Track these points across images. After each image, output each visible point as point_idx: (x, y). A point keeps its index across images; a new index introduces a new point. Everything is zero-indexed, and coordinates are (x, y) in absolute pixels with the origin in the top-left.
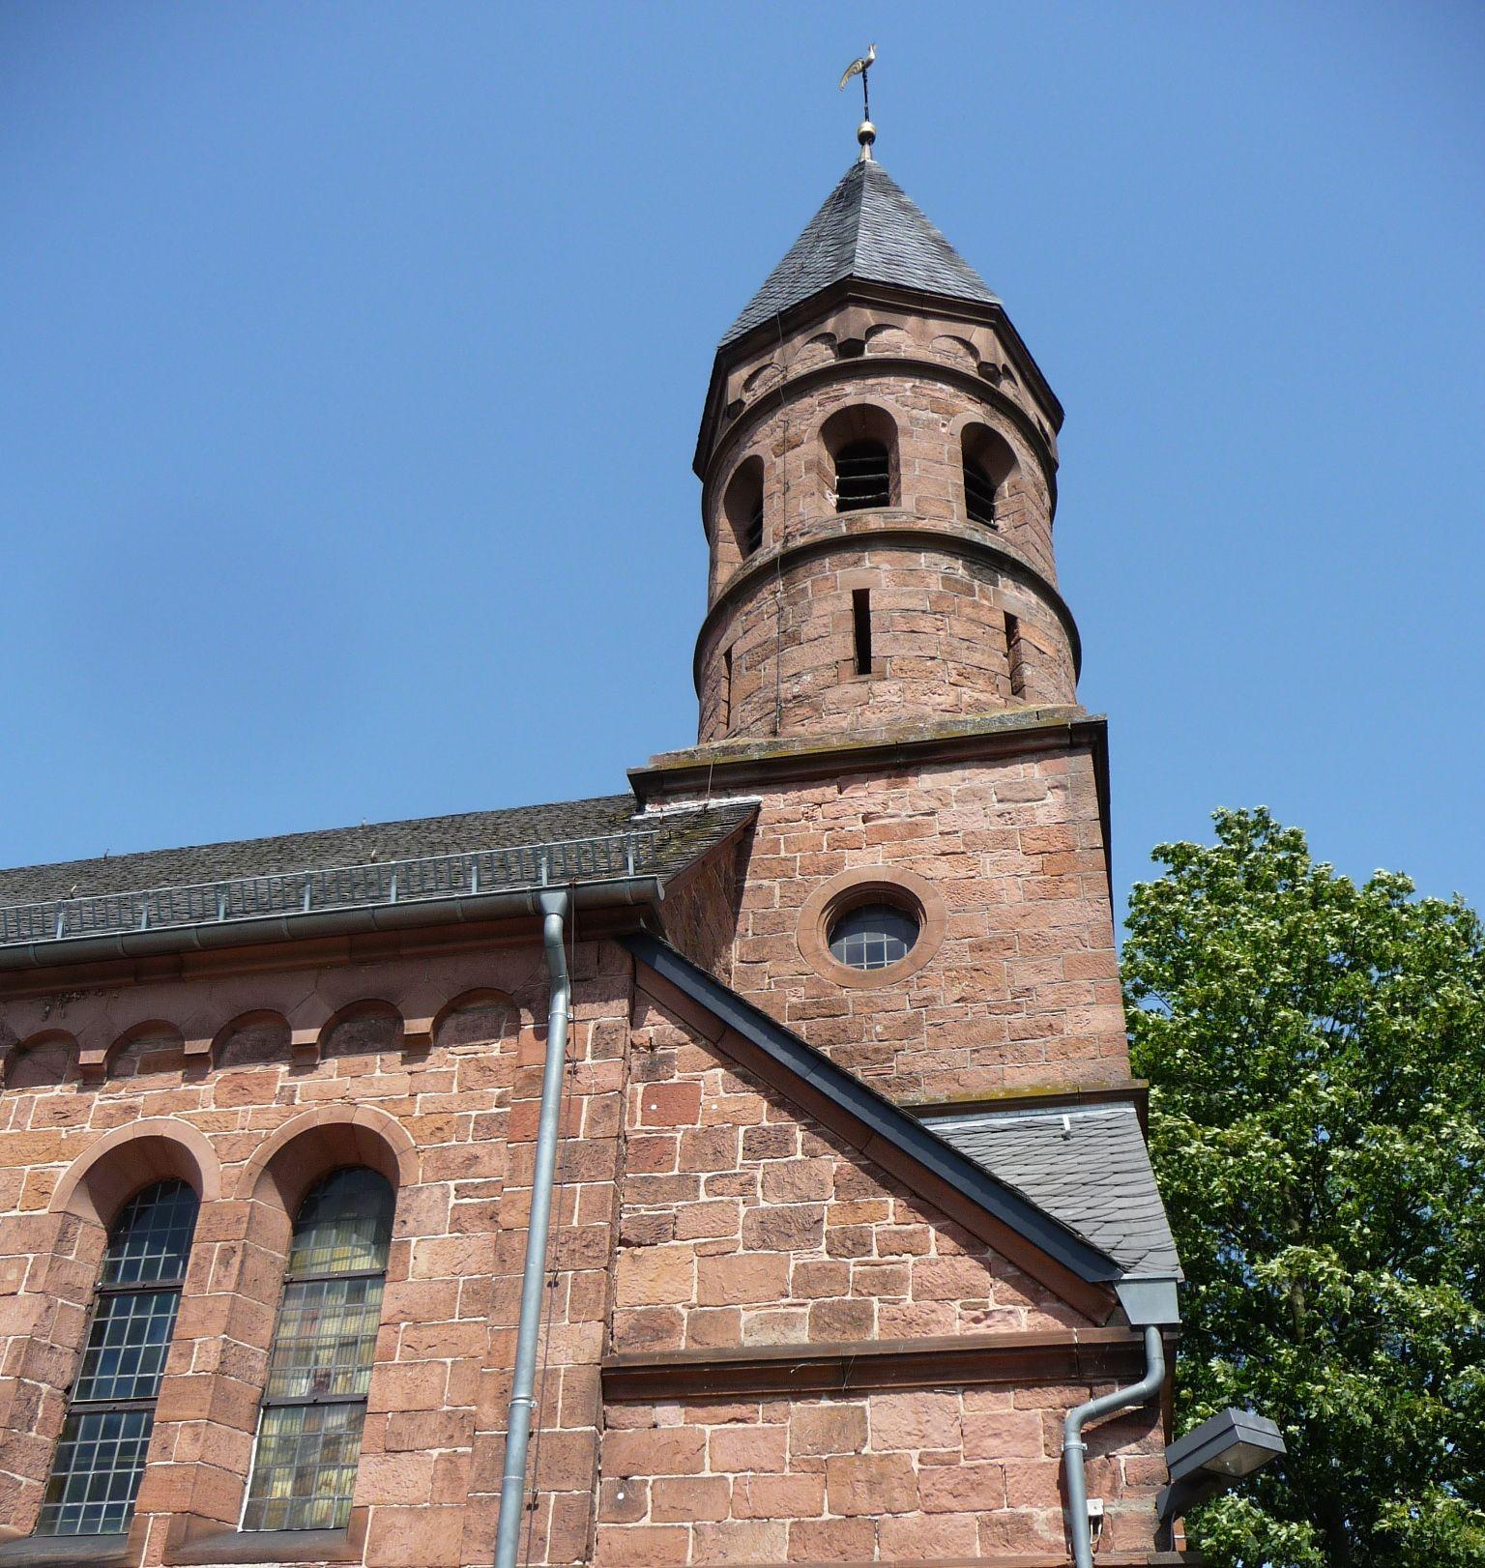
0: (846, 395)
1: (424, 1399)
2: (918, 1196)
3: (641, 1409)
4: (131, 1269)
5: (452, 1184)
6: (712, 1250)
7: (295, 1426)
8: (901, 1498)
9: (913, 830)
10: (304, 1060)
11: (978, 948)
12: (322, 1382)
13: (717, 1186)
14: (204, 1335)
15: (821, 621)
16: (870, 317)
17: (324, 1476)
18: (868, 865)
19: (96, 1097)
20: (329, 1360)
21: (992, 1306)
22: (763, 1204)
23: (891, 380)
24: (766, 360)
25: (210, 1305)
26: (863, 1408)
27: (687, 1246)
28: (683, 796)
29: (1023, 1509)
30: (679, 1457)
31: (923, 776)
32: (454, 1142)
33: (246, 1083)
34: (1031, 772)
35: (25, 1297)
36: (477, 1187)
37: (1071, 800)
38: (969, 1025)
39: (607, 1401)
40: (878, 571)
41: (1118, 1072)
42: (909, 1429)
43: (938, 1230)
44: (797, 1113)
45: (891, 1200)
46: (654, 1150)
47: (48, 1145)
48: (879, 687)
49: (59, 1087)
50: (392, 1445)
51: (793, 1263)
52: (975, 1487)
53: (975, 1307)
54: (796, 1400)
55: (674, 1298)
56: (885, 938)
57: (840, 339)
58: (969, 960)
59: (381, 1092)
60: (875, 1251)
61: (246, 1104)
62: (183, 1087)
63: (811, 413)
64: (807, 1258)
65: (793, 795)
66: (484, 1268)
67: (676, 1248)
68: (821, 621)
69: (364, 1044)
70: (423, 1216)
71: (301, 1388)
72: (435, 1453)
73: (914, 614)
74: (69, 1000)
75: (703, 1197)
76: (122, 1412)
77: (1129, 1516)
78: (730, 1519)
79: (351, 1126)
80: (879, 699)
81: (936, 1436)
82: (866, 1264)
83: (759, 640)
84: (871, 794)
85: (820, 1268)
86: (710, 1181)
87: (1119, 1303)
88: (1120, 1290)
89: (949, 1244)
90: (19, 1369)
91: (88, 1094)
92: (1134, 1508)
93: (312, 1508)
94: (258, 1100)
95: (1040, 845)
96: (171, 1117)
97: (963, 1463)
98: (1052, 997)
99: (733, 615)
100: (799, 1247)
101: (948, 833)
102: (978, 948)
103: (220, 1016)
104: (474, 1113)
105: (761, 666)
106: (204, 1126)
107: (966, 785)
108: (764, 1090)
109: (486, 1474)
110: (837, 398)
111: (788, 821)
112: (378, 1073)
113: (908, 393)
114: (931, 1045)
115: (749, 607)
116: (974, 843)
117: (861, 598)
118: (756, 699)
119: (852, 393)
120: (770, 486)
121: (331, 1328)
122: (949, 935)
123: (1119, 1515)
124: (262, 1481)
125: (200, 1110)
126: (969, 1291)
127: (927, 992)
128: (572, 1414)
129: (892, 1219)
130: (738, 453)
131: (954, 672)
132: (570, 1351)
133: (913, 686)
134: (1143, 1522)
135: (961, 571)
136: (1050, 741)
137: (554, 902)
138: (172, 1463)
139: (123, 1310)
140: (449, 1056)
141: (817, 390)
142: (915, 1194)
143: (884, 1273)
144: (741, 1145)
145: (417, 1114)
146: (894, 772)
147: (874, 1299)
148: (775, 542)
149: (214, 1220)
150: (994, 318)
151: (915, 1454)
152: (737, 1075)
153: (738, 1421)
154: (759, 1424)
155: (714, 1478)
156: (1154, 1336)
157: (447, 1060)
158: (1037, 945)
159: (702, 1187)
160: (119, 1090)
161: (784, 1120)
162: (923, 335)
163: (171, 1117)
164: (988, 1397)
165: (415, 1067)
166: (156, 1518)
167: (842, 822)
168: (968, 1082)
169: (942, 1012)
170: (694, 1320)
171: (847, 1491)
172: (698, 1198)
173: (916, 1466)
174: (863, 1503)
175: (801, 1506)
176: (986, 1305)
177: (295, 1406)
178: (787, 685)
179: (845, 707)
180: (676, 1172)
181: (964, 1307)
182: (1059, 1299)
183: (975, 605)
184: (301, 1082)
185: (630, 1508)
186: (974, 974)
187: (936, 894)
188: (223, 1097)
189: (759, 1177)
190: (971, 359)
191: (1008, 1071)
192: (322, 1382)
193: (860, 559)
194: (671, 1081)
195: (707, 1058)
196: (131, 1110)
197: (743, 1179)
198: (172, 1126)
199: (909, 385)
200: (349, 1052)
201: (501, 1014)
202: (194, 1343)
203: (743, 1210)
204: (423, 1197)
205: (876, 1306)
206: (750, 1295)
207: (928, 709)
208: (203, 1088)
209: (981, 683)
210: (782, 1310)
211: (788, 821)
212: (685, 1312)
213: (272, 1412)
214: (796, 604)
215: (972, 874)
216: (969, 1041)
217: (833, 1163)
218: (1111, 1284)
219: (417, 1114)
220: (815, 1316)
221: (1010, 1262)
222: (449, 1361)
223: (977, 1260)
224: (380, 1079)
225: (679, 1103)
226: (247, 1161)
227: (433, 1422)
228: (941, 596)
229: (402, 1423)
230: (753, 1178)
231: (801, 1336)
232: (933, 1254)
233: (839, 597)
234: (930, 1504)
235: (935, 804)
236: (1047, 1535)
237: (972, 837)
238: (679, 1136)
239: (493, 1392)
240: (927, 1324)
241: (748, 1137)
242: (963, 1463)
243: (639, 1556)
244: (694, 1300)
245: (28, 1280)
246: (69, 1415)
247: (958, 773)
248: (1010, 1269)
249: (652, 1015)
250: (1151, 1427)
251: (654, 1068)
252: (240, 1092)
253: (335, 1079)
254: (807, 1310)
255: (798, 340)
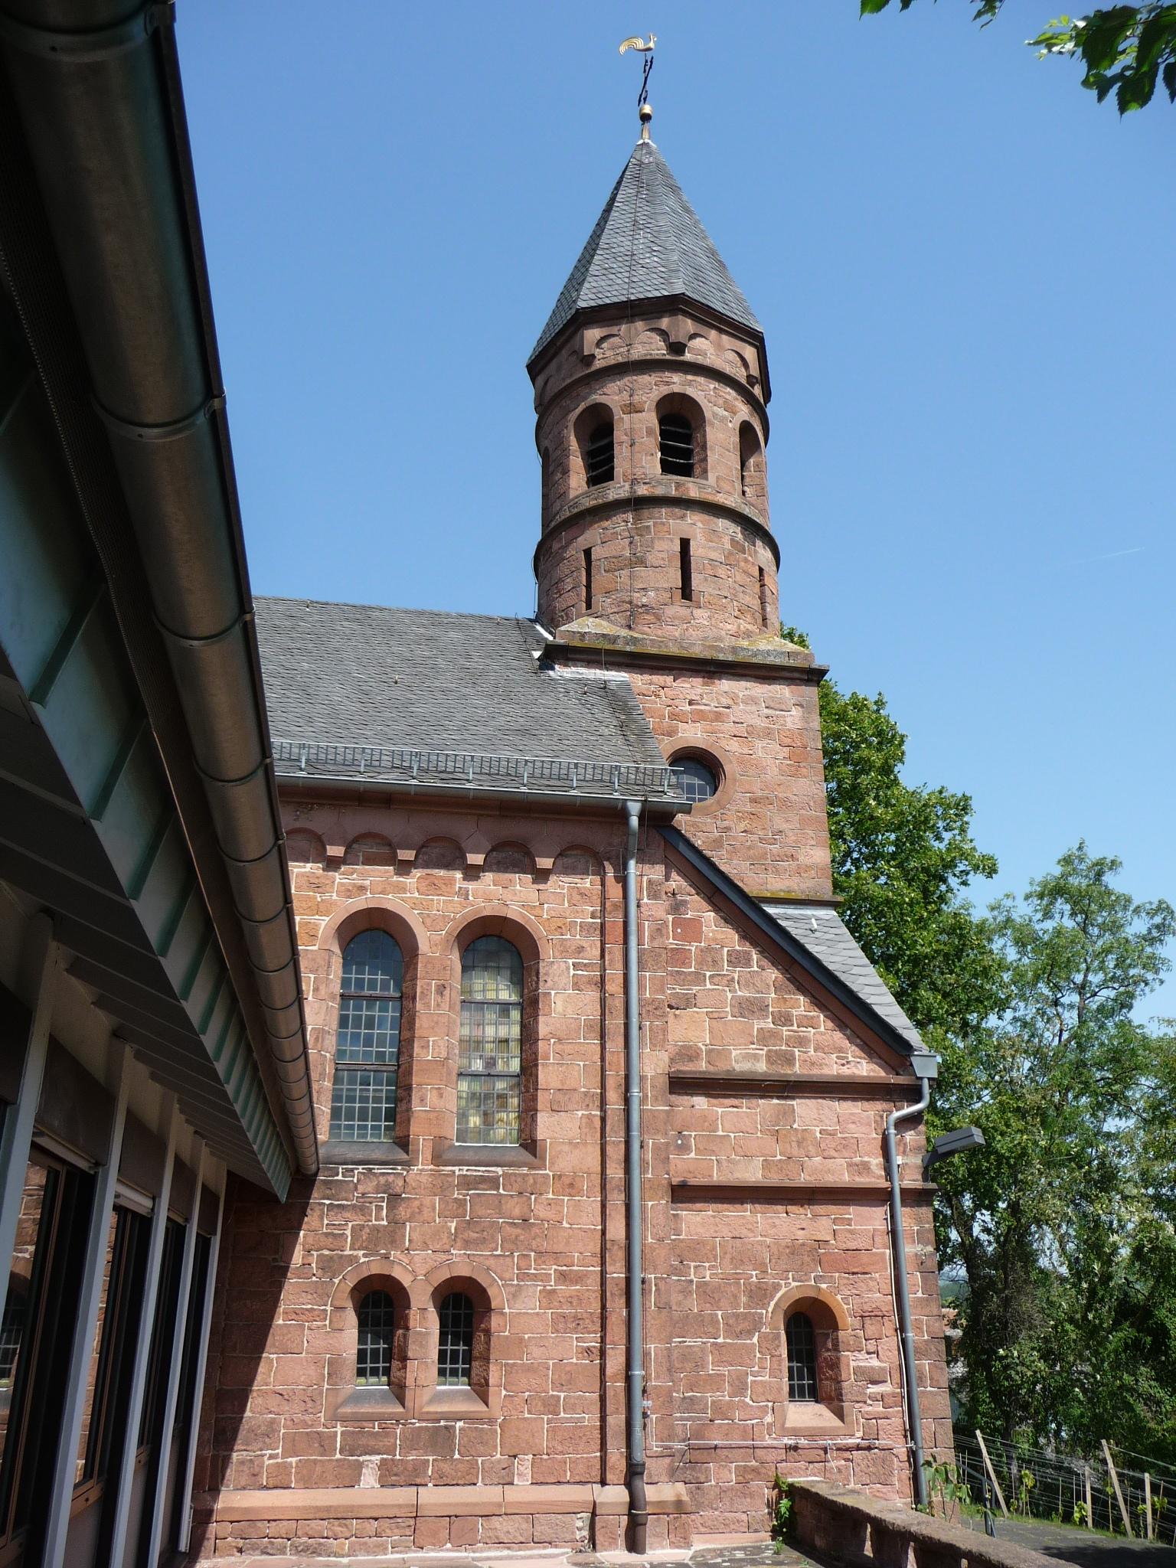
0: (674, 383)
1: (570, 1084)
2: (816, 998)
3: (686, 1097)
4: (360, 983)
5: (570, 961)
6: (716, 1015)
7: (477, 1087)
8: (812, 1150)
9: (718, 717)
10: (472, 873)
11: (754, 801)
12: (491, 1063)
13: (716, 980)
14: (435, 1036)
15: (660, 555)
16: (689, 326)
17: (498, 1116)
18: (692, 735)
19: (338, 877)
20: (491, 1050)
21: (851, 1059)
22: (739, 993)
23: (701, 380)
24: (614, 330)
25: (435, 1019)
26: (793, 1105)
27: (703, 1012)
28: (579, 664)
29: (866, 1159)
30: (706, 1124)
31: (724, 681)
32: (569, 937)
33: (436, 882)
34: (783, 692)
35: (314, 1002)
36: (585, 965)
37: (805, 715)
38: (749, 848)
39: (670, 1093)
40: (695, 525)
41: (826, 892)
42: (815, 1117)
43: (825, 1016)
44: (754, 944)
45: (802, 998)
46: (678, 956)
47: (310, 904)
48: (697, 612)
49: (309, 865)
50: (555, 1107)
51: (756, 1027)
52: (845, 1147)
53: (842, 1058)
54: (761, 1098)
55: (697, 1040)
56: (697, 781)
57: (672, 339)
58: (749, 808)
59: (522, 900)
60: (795, 1025)
61: (438, 895)
62: (395, 878)
63: (651, 389)
64: (763, 1025)
65: (647, 677)
66: (595, 1013)
67: (697, 1013)
68: (660, 555)
69: (508, 867)
70: (556, 979)
71: (478, 1066)
72: (580, 1113)
73: (716, 563)
74: (312, 809)
75: (709, 986)
76: (370, 1071)
77: (910, 1164)
78: (733, 1156)
79: (505, 918)
80: (697, 621)
81: (827, 1122)
82: (792, 1031)
83: (614, 553)
84: (691, 687)
85: (770, 1031)
86: (711, 977)
87: (911, 1065)
88: (912, 1059)
89: (830, 1024)
90: (319, 1046)
91: (330, 873)
92: (913, 1161)
93: (494, 1133)
94: (446, 894)
95: (788, 741)
96: (390, 896)
97: (839, 1135)
98: (794, 838)
99: (591, 524)
100: (758, 1019)
101: (738, 723)
102: (754, 801)
103: (419, 838)
104: (579, 920)
105: (617, 573)
106: (413, 906)
107: (747, 693)
108: (737, 928)
109: (615, 1129)
110: (668, 383)
111: (644, 695)
112: (518, 887)
113: (712, 393)
114: (729, 857)
115: (606, 524)
116: (751, 731)
117: (685, 544)
118: (614, 597)
119: (678, 382)
120: (619, 435)
121: (490, 1032)
122: (739, 790)
123: (906, 1164)
124: (463, 1116)
125: (409, 895)
126: (841, 1050)
127: (726, 823)
128: (657, 1099)
129: (803, 1008)
130: (590, 394)
131: (737, 609)
132: (652, 1066)
133: (716, 616)
134: (917, 1168)
135: (740, 536)
136: (797, 675)
137: (634, 808)
138: (428, 1109)
139: (358, 1008)
140: (560, 883)
141: (654, 372)
142: (813, 996)
143: (800, 1036)
144: (725, 958)
145: (545, 916)
146: (706, 675)
147: (796, 1050)
148: (624, 481)
149: (429, 966)
150: (756, 339)
151: (818, 1129)
152: (721, 917)
153: (733, 1107)
154: (744, 1110)
155: (724, 1136)
156: (926, 1082)
157: (560, 885)
158: (785, 805)
159: (707, 980)
160: (352, 874)
161: (747, 947)
162: (719, 347)
163: (390, 896)
164: (849, 1103)
165: (541, 887)
166: (424, 1139)
167: (676, 702)
168: (748, 883)
169: (734, 837)
170: (709, 1052)
171: (788, 1146)
172: (705, 985)
173: (818, 1135)
174: (795, 1151)
175: (767, 1152)
176: (847, 1058)
177: (475, 1076)
178: (637, 595)
179: (676, 622)
180: (693, 969)
181: (837, 1057)
182: (880, 1058)
183: (746, 561)
184: (471, 886)
185: (684, 1148)
186: (752, 816)
187: (731, 762)
188: (423, 889)
189: (736, 978)
190: (743, 370)
191: (769, 879)
192: (491, 1063)
193: (683, 517)
194: (687, 916)
195: (705, 905)
196: (362, 889)
197: (729, 978)
198: (391, 902)
199: (712, 386)
200: (499, 871)
201: (587, 862)
202: (429, 1041)
203: (730, 995)
204: (555, 967)
205: (797, 1053)
206: (736, 1042)
207: (723, 633)
208: (408, 881)
209: (749, 618)
210: (751, 1051)
211: (644, 695)
212: (703, 1048)
213: (462, 1077)
214: (641, 535)
215: (751, 752)
216: (749, 858)
217: (773, 974)
218: (909, 1056)
219: (545, 916)
220: (768, 1056)
221: (858, 1037)
222: (582, 1063)
223: (844, 1034)
224: (521, 891)
225: (690, 930)
226: (444, 932)
227: (576, 1097)
228: (731, 554)
229: (560, 1096)
230: (733, 978)
231: (761, 1067)
232: (822, 1029)
233: (672, 540)
234: (826, 1154)
235: (730, 702)
236: (877, 1172)
237: (751, 728)
238: (693, 949)
239: (614, 1085)
240: (821, 1065)
241: (729, 954)
242: (839, 1135)
243: (690, 1172)
244: (708, 1042)
245: (313, 991)
246: (336, 1070)
247: (743, 684)
248: (858, 1041)
249: (674, 875)
250: (920, 1124)
251: (677, 908)
252: (434, 886)
253: (492, 887)
254: (764, 1052)
255: (640, 325)
